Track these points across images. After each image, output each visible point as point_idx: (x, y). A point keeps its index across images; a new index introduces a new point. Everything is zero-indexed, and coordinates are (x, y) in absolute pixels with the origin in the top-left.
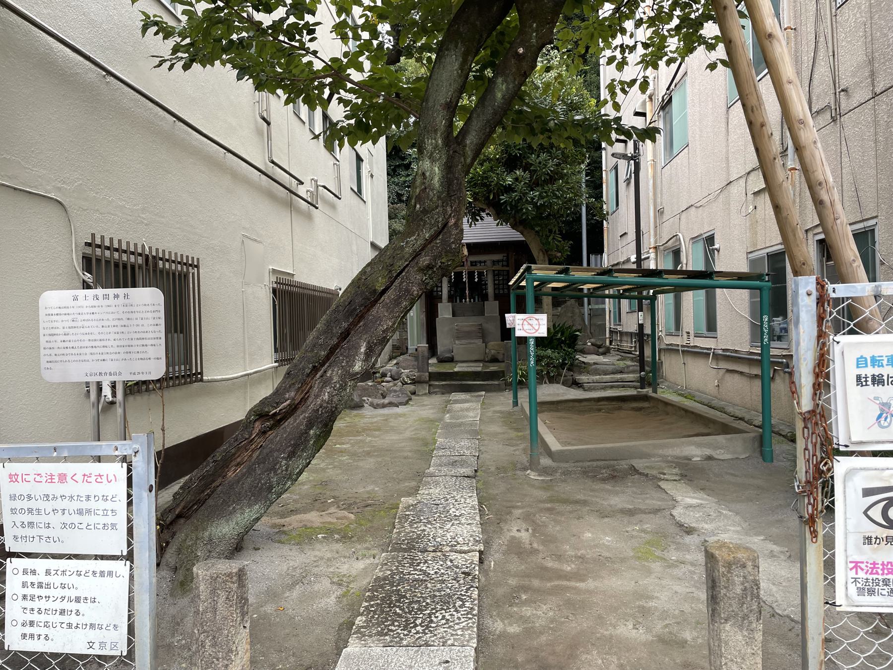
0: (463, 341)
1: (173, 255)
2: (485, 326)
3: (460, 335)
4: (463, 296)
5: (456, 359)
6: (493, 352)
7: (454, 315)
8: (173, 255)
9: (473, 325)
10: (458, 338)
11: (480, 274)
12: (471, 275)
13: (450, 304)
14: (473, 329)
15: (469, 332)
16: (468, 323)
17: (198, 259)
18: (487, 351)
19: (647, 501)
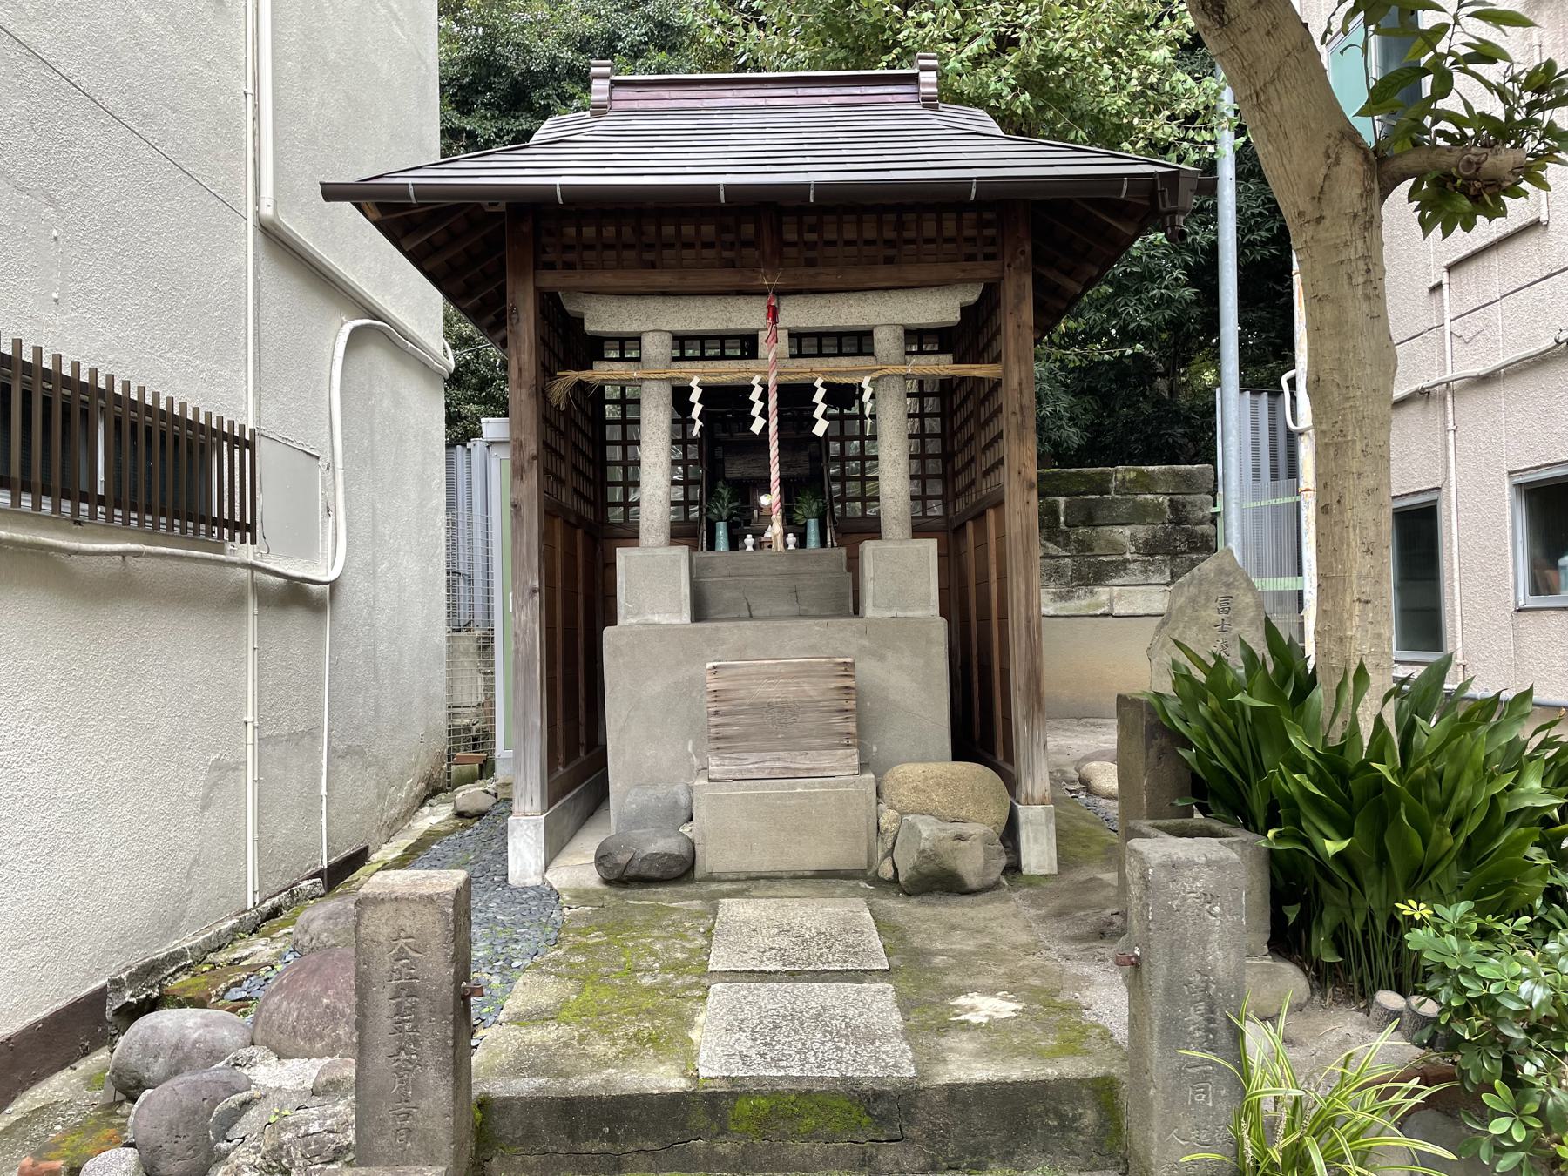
0: (751, 762)
1: (237, 535)
2: (869, 670)
3: (731, 726)
4: (744, 523)
5: (709, 861)
6: (928, 830)
7: (700, 610)
8: (237, 535)
9: (806, 672)
10: (722, 742)
11: (843, 396)
12: (795, 398)
13: (681, 552)
14: (811, 689)
15: (784, 711)
16: (777, 655)
17: (253, 432)
18: (888, 818)
19: (1018, 519)
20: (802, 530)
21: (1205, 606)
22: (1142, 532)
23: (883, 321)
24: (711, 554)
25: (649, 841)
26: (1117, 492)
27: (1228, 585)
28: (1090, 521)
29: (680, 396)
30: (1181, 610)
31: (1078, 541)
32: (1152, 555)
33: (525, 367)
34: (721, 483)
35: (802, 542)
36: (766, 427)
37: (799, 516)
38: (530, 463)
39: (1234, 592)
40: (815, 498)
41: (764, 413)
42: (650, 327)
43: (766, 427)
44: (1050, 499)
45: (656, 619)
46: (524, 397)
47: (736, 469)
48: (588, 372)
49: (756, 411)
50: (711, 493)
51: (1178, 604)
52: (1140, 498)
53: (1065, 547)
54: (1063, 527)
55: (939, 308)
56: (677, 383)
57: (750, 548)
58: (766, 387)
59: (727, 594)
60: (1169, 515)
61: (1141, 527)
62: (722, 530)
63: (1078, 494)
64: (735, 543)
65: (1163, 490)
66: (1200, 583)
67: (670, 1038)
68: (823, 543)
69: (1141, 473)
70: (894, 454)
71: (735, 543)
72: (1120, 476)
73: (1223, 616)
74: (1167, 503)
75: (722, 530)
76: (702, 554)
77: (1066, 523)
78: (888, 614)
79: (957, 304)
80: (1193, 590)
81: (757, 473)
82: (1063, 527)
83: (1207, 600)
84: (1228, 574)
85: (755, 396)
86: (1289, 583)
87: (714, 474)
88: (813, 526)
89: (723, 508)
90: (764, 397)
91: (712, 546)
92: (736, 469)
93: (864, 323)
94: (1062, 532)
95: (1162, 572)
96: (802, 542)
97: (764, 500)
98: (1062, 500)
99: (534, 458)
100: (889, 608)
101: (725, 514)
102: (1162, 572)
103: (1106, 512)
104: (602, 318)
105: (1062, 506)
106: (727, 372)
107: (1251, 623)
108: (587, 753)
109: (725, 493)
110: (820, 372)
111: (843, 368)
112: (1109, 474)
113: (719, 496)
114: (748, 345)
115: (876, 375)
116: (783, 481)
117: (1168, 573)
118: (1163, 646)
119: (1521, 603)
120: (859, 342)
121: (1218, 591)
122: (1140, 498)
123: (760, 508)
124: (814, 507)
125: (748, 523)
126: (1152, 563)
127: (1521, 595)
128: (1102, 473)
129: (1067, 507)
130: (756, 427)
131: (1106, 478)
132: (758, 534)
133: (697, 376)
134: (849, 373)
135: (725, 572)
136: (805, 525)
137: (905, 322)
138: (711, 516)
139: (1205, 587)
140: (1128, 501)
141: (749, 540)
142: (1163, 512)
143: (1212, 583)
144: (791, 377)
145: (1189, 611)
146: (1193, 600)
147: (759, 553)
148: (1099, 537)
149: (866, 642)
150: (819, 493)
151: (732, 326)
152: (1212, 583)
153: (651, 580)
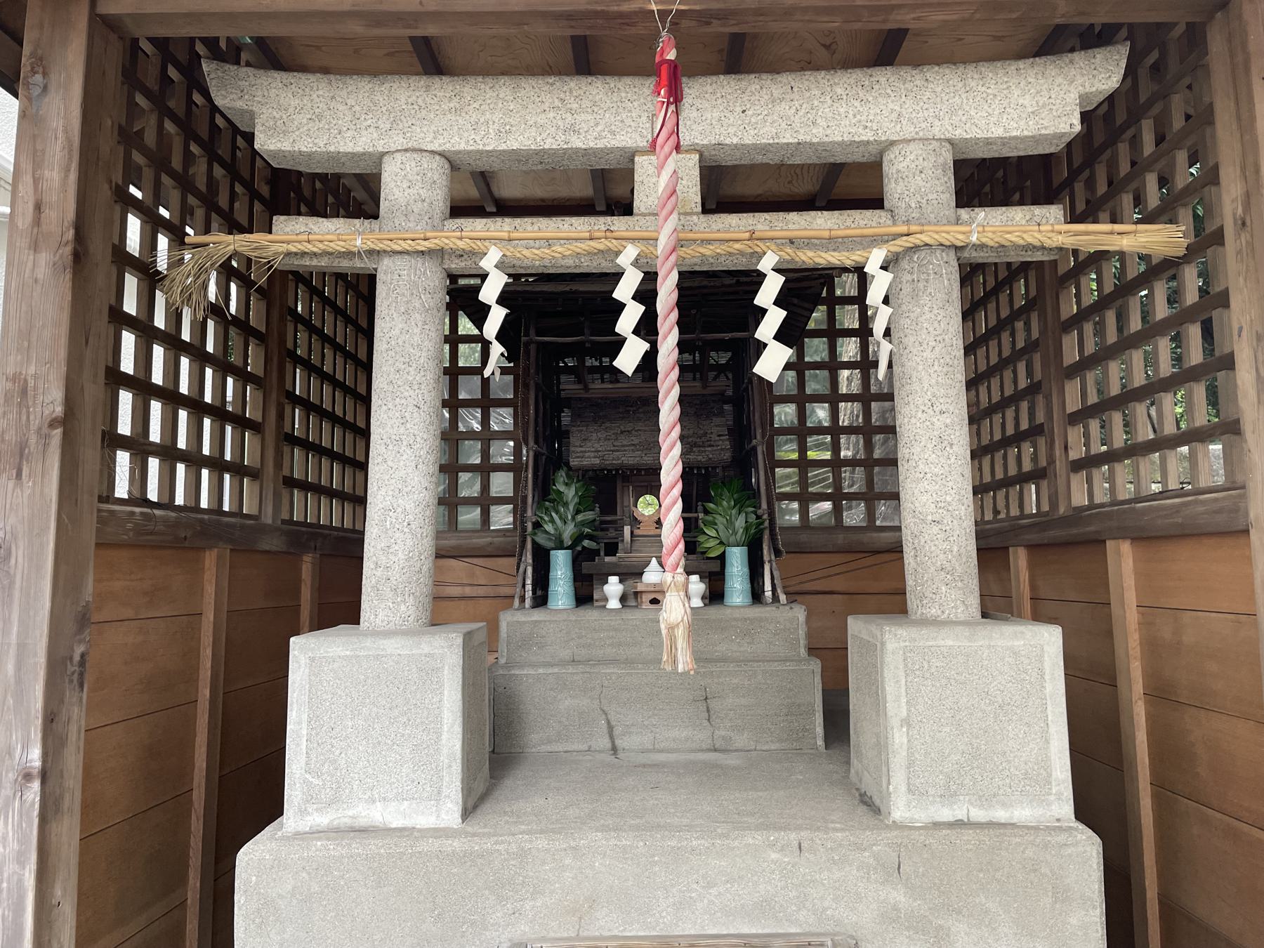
12: (716, 304)
20: (715, 567)
23: (909, 131)
24: (538, 615)
29: (463, 298)
33: (52, 197)
34: (561, 476)
35: (715, 595)
36: (649, 361)
37: (709, 543)
38: (45, 439)
40: (740, 505)
41: (647, 328)
42: (397, 141)
43: (649, 361)
45: (377, 814)
46: (43, 271)
47: (591, 448)
48: (258, 238)
49: (627, 322)
50: (544, 491)
55: (1037, 106)
56: (456, 265)
57: (614, 604)
58: (650, 278)
59: (567, 703)
62: (561, 564)
64: (584, 595)
68: (756, 596)
70: (939, 421)
71: (584, 595)
75: (561, 564)
76: (520, 617)
78: (946, 814)
79: (1073, 97)
81: (630, 458)
85: (624, 291)
87: (545, 466)
88: (737, 561)
89: (564, 523)
90: (646, 295)
91: (541, 600)
92: (591, 448)
93: (868, 136)
96: (715, 595)
97: (645, 507)
99: (53, 424)
100: (949, 796)
101: (569, 531)
104: (296, 121)
106: (560, 243)
109: (570, 494)
110: (772, 246)
111: (818, 235)
113: (559, 500)
114: (605, 191)
115: (897, 246)
116: (688, 475)
120: (847, 184)
123: (635, 522)
124: (740, 523)
125: (612, 549)
130: (628, 359)
132: (631, 574)
133: (498, 251)
134: (832, 242)
135: (565, 654)
136: (722, 558)
137: (959, 133)
138: (541, 539)
141: (613, 587)
144: (707, 251)
147: (634, 616)
149: (898, 896)
150: (748, 496)
151: (577, 143)
153: (368, 712)
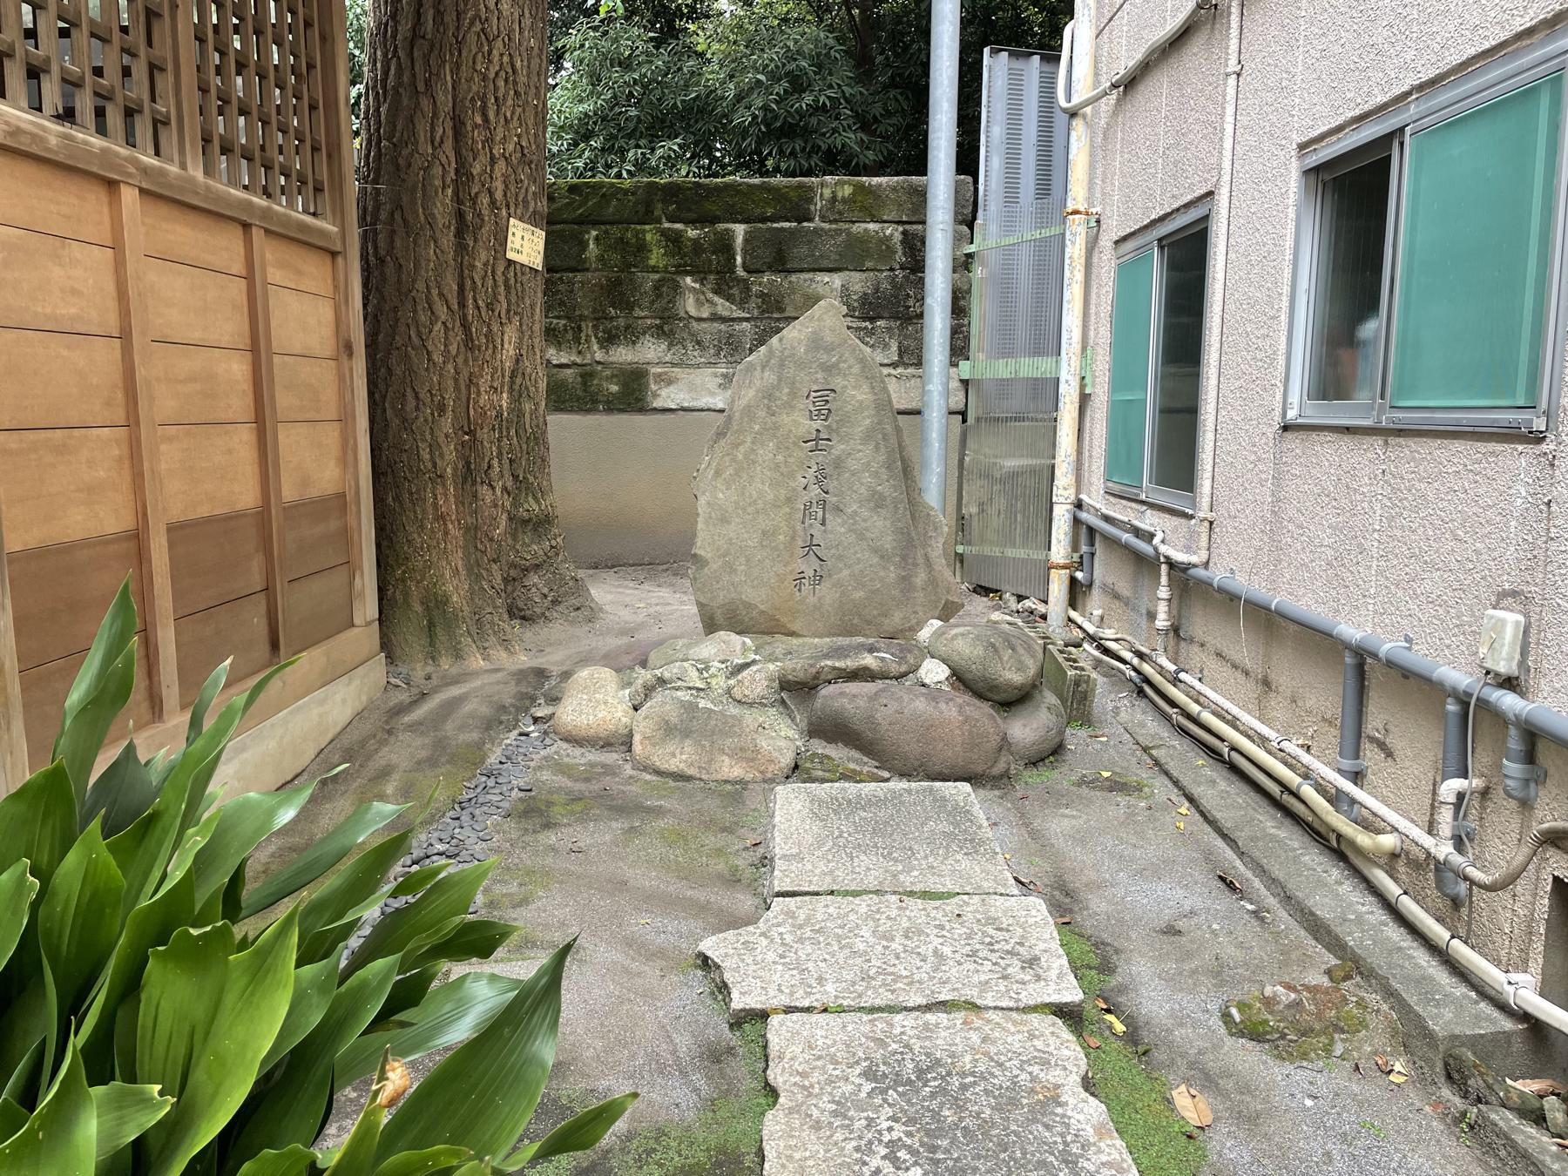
21: (789, 406)
22: (858, 282)
25: (356, 818)
26: (823, 219)
27: (828, 369)
28: (780, 264)
30: (748, 411)
31: (762, 295)
32: (872, 320)
39: (838, 382)
44: (721, 226)
51: (743, 402)
52: (858, 228)
53: (742, 304)
54: (740, 272)
60: (900, 257)
61: (857, 276)
63: (764, 220)
65: (893, 216)
66: (782, 365)
67: (1465, 997)
69: (860, 188)
72: (827, 192)
73: (818, 424)
74: (898, 237)
77: (745, 267)
80: (770, 377)
82: (740, 272)
83: (793, 394)
84: (829, 350)
86: (1030, 367)
94: (739, 280)
95: (886, 346)
98: (740, 230)
102: (886, 346)
103: (804, 250)
105: (739, 240)
107: (868, 437)
108: (131, 652)
112: (811, 188)
117: (894, 347)
118: (718, 473)
119: (1292, 414)
121: (810, 380)
122: (858, 228)
126: (871, 333)
127: (1294, 399)
128: (800, 186)
129: (746, 241)
131: (807, 194)
139: (790, 371)
140: (838, 232)
142: (891, 251)
143: (801, 365)
145: (762, 414)
146: (769, 395)
148: (793, 290)
152: (801, 365)
